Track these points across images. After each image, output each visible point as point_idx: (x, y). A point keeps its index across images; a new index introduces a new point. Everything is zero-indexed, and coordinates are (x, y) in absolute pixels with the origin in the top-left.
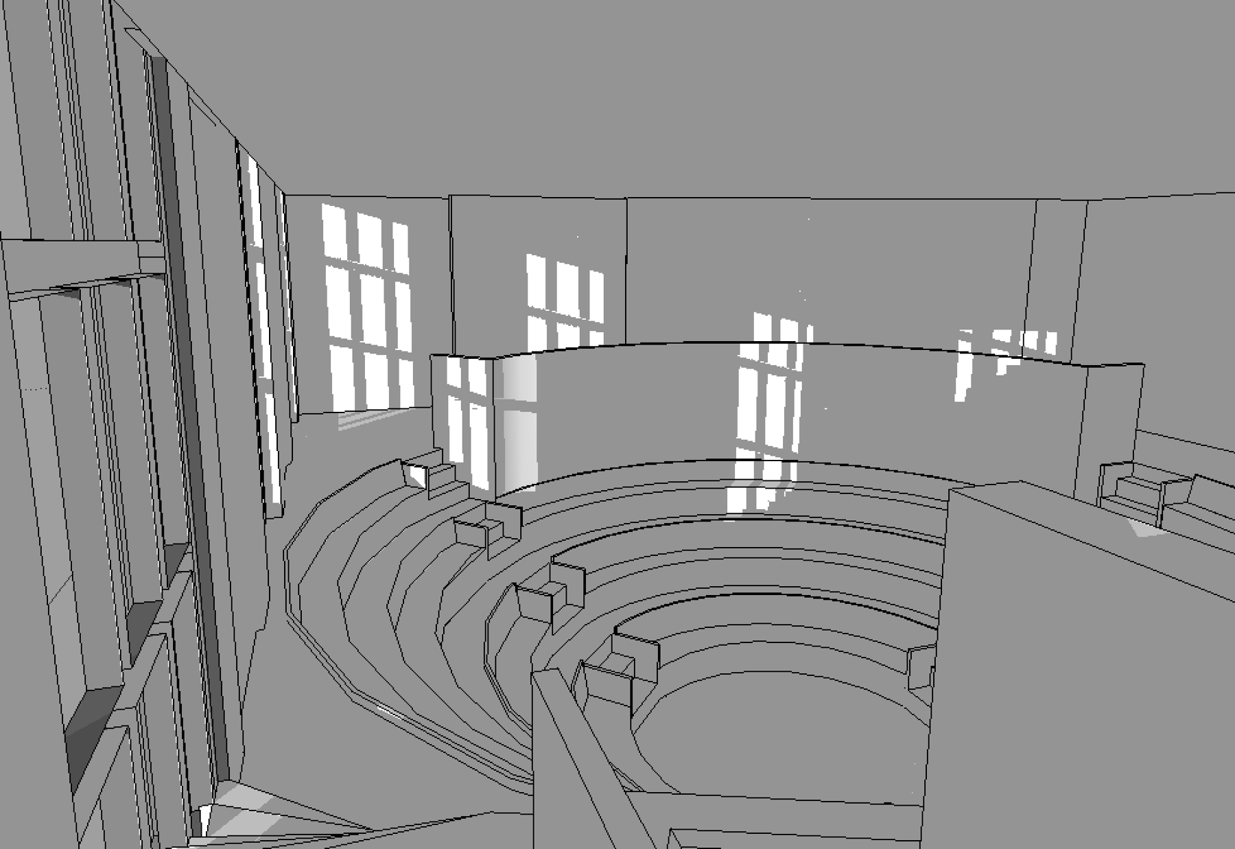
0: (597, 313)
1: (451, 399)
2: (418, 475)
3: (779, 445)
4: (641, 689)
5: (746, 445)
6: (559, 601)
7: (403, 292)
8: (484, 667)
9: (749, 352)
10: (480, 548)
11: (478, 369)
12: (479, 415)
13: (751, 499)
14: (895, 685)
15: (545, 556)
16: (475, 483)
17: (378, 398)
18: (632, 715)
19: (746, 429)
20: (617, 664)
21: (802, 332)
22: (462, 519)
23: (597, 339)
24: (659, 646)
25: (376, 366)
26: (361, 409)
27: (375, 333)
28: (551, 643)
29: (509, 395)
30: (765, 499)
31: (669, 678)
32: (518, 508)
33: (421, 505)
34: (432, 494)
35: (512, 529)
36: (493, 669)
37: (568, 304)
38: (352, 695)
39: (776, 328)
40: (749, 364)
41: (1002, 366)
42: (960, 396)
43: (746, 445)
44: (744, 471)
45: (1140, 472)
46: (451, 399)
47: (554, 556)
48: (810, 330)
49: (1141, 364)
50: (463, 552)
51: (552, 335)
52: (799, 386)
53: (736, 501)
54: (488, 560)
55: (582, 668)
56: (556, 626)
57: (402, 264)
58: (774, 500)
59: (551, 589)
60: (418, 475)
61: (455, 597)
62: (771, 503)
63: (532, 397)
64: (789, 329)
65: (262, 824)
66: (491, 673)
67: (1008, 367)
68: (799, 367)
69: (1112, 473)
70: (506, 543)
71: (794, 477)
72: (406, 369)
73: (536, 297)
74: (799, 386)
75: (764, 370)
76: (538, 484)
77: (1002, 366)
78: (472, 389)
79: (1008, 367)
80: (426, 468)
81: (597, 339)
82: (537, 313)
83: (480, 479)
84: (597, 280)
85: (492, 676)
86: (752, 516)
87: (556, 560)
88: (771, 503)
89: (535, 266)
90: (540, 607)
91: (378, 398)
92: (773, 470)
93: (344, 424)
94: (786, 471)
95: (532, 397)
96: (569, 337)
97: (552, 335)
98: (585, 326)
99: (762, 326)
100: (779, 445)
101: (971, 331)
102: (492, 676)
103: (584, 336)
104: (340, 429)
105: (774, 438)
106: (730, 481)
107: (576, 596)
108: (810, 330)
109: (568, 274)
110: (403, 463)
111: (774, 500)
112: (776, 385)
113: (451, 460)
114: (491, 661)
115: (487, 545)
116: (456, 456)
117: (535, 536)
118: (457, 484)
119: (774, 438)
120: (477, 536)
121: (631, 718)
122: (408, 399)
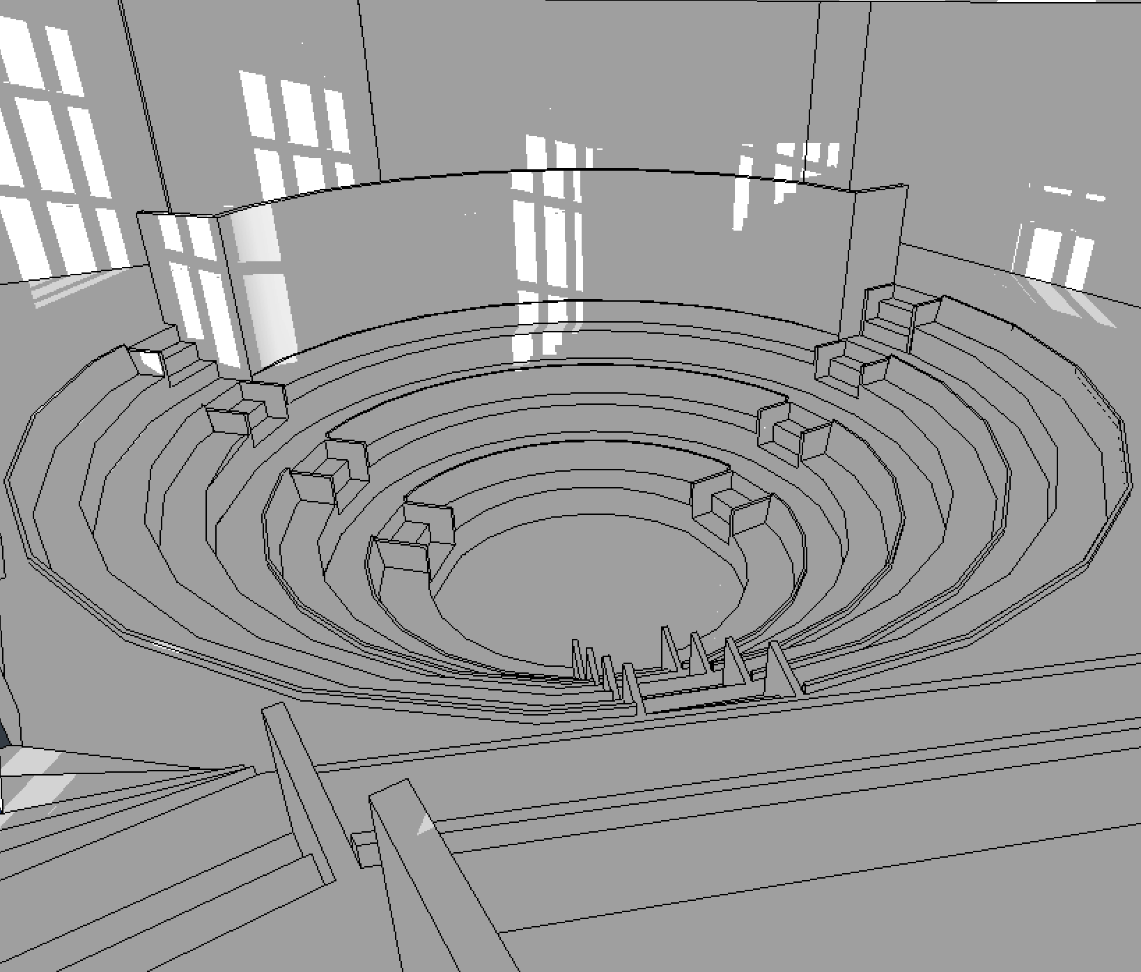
0: (341, 141)
1: (173, 266)
2: (151, 362)
3: (563, 284)
4: (437, 553)
5: (528, 286)
6: (340, 480)
7: (81, 120)
8: (268, 565)
9: (522, 182)
10: (244, 435)
11: (200, 230)
12: (213, 283)
13: (538, 346)
14: (681, 515)
15: (319, 433)
16: (222, 360)
17: (79, 258)
18: (430, 579)
19: (526, 270)
20: (410, 533)
21: (581, 156)
22: (215, 405)
23: (345, 175)
24: (452, 509)
25: (66, 219)
26: (59, 274)
27: (55, 176)
28: (338, 523)
29: (243, 259)
30: (551, 344)
31: (466, 538)
32: (280, 385)
33: (163, 395)
34: (174, 380)
35: (277, 407)
36: (280, 569)
37: (303, 131)
38: (124, 635)
39: (551, 151)
40: (523, 196)
41: (781, 191)
42: (738, 226)
43: (528, 286)
44: (528, 315)
45: (900, 293)
46: (173, 266)
47: (328, 433)
48: (589, 153)
49: (901, 185)
50: (221, 444)
51: (289, 174)
52: (578, 217)
53: (522, 349)
54: (254, 447)
55: (374, 543)
56: (341, 506)
57: (71, 83)
58: (560, 343)
59: (328, 468)
60: (151, 362)
61: (221, 494)
62: (557, 347)
63: (276, 256)
64: (567, 154)
65: (53, 789)
66: (278, 573)
67: (786, 195)
68: (578, 198)
69: (875, 296)
70: (271, 424)
71: (580, 316)
72: (108, 220)
73: (261, 124)
74: (578, 217)
75: (539, 199)
76: (299, 353)
77: (781, 191)
78: (198, 254)
79: (786, 195)
80: (159, 352)
81: (345, 175)
82: (265, 144)
83: (229, 355)
84: (334, 101)
85: (279, 576)
86: (539, 363)
87: (332, 435)
88: (557, 347)
89: (253, 86)
90: (320, 489)
91: (79, 258)
92: (558, 312)
93: (42, 298)
94: (571, 312)
95: (276, 256)
96: (310, 176)
97: (289, 174)
98: (329, 158)
99: (535, 150)
100: (563, 284)
101: (751, 146)
102: (279, 576)
103: (329, 172)
104: (38, 305)
105: (556, 278)
106: (514, 326)
107: (359, 470)
108: (589, 153)
109: (297, 95)
110: (128, 349)
111: (560, 343)
112: (555, 219)
113: (189, 336)
114: (275, 558)
115: (250, 429)
116: (194, 331)
117: (301, 413)
118: (201, 365)
119: (556, 278)
120: (238, 424)
121: (429, 583)
122: (119, 256)
